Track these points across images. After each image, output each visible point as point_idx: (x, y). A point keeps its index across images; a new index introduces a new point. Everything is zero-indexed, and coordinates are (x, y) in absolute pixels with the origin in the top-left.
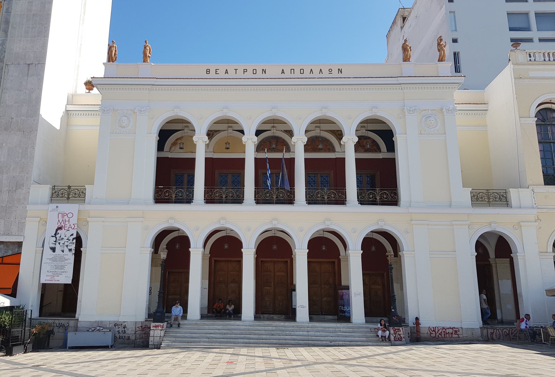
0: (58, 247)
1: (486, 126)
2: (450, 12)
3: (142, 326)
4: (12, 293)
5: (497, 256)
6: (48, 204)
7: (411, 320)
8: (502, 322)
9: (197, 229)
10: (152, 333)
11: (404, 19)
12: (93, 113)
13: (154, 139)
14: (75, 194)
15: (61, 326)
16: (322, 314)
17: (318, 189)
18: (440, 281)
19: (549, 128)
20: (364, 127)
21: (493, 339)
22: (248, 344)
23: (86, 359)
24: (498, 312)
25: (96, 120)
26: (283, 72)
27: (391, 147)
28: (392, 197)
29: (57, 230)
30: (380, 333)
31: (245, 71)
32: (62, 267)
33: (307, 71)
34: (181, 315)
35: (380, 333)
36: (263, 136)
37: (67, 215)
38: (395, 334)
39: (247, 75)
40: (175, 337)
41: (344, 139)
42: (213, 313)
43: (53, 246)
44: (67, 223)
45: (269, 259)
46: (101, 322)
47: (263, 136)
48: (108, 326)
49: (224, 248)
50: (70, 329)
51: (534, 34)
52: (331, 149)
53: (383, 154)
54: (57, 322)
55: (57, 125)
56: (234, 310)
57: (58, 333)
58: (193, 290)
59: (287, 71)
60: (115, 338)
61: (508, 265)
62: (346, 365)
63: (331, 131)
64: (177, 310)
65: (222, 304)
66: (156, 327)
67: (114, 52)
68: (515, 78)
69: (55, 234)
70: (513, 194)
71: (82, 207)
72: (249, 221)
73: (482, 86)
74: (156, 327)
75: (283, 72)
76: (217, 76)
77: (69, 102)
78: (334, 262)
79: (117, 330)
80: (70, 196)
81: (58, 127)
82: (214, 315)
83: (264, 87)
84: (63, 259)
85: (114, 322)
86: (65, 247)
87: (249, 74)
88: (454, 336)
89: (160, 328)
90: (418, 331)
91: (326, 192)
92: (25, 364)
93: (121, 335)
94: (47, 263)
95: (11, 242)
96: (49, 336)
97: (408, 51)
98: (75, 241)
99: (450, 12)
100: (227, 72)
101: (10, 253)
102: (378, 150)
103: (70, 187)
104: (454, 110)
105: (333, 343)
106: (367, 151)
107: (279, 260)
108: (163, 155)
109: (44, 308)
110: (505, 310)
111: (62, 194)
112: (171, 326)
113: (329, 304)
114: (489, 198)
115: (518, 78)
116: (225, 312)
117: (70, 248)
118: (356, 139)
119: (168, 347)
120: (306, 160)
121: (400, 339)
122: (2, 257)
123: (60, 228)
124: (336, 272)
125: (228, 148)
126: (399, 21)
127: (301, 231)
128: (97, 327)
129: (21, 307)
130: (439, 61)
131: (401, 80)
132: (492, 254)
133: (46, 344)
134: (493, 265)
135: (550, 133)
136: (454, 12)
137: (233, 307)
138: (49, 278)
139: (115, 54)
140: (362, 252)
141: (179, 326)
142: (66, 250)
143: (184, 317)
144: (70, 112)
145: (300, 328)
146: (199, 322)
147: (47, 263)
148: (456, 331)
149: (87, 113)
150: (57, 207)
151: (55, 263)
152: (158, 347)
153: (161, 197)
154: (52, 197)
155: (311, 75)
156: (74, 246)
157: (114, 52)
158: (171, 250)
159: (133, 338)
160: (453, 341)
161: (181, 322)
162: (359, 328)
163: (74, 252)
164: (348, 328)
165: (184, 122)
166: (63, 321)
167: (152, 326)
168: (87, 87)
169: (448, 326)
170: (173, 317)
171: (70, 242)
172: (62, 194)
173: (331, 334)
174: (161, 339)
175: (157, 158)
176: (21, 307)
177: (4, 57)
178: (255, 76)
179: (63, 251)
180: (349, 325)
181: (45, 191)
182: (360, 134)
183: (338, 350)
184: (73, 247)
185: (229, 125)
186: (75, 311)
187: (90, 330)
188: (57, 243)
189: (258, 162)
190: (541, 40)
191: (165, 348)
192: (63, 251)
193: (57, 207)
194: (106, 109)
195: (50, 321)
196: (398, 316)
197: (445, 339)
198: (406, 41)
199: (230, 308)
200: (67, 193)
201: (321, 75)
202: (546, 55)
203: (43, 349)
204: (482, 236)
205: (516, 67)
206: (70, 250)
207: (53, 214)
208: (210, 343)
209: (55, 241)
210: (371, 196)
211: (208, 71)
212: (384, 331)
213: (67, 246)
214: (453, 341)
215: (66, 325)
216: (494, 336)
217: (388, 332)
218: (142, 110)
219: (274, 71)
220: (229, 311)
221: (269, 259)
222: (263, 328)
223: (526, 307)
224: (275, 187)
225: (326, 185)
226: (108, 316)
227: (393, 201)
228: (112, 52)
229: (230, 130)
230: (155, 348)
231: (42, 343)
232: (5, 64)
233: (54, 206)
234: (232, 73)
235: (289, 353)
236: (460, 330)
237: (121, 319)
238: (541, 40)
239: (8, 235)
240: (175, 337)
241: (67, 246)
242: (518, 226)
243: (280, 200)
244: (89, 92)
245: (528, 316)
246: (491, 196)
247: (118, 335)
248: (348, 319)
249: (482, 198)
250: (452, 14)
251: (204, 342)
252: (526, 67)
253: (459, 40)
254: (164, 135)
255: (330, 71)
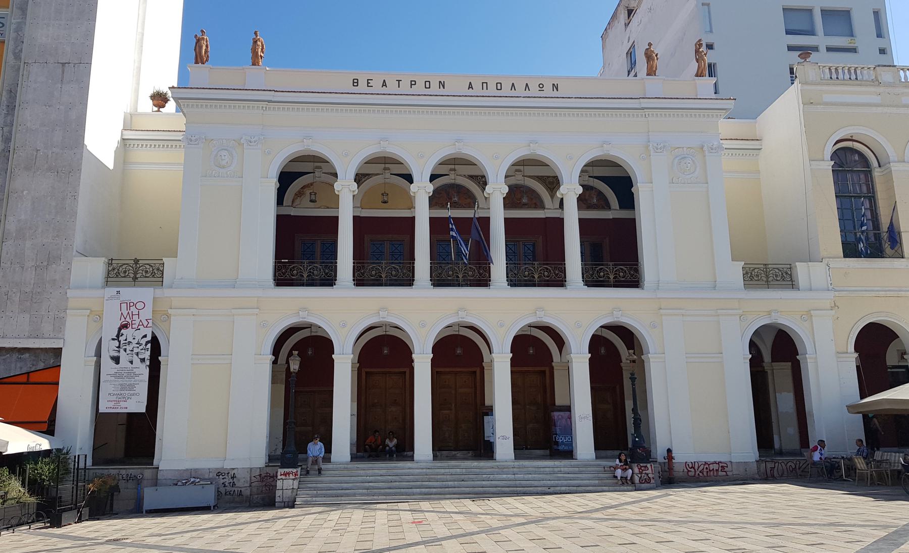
0: (122, 355)
1: (758, 172)
2: (703, 4)
3: (260, 475)
4: (48, 429)
5: (774, 359)
6: (103, 287)
7: (660, 452)
8: (781, 453)
9: (344, 326)
10: (279, 484)
11: (630, 12)
12: (170, 143)
13: (272, 185)
14: (146, 272)
15: (129, 478)
16: (527, 449)
17: (293, 263)
18: (697, 396)
19: (849, 176)
20: (519, 171)
21: (773, 476)
22: (427, 496)
23: (186, 527)
24: (776, 438)
25: (178, 156)
26: (470, 86)
27: (627, 199)
28: (632, 275)
29: (120, 329)
30: (619, 473)
31: (413, 83)
32: (131, 387)
33: (520, 87)
34: (322, 456)
35: (619, 473)
36: (440, 182)
37: (135, 305)
38: (641, 473)
39: (417, 89)
40: (315, 489)
41: (488, 189)
42: (365, 451)
43: (116, 354)
44: (135, 317)
45: (448, 370)
46: (196, 470)
47: (440, 182)
48: (207, 476)
49: (384, 354)
50: (145, 482)
51: (820, 40)
52: (538, 203)
53: (615, 212)
54: (123, 472)
55: (109, 161)
56: (397, 446)
57: (127, 491)
58: (338, 416)
59: (477, 85)
60: (219, 494)
61: (789, 372)
62: (592, 519)
63: (538, 177)
64: (315, 448)
65: (384, 437)
66: (285, 474)
67: (204, 48)
68: (804, 104)
69: (118, 336)
70: (802, 270)
71: (159, 292)
72: (422, 312)
73: (753, 115)
74: (285, 474)
75: (470, 86)
76: (369, 90)
77: (128, 125)
78: (544, 372)
79: (222, 481)
80: (770, 279)
81: (111, 166)
82: (366, 455)
83: (584, 112)
84: (131, 375)
85: (217, 469)
86: (135, 356)
87: (419, 88)
88: (720, 473)
89: (291, 477)
90: (671, 468)
91: (609, 270)
92: (92, 539)
93: (229, 489)
94: (107, 381)
95: (42, 349)
96: (112, 495)
97: (653, 60)
98: (149, 346)
99: (703, 4)
100: (384, 84)
101: (41, 365)
102: (606, 206)
103: (138, 260)
104: (720, 147)
105: (552, 489)
106: (590, 207)
107: (530, 369)
108: (286, 211)
109: (101, 452)
110: (785, 434)
111: (125, 272)
112: (308, 472)
113: (541, 433)
114: (767, 277)
115: (808, 103)
116: (383, 450)
117: (142, 357)
118: (506, 190)
119: (307, 504)
120: (507, 220)
121: (648, 481)
122: (28, 373)
123: (124, 326)
124: (548, 385)
125: (385, 202)
126: (623, 16)
127: (502, 326)
128: (190, 478)
129: (65, 451)
130: (697, 75)
131: (645, 103)
132: (767, 357)
133: (108, 508)
134: (769, 372)
135: (850, 183)
136: (708, 5)
137: (395, 441)
138: (111, 404)
139: (206, 51)
140: (856, 355)
141: (320, 473)
142: (136, 360)
143: (327, 459)
144: (128, 142)
145: (502, 469)
146: (350, 466)
147: (107, 381)
148: (723, 466)
149: (157, 143)
150: (118, 292)
151: (120, 381)
152: (291, 505)
153: (283, 278)
154: (108, 277)
155: (513, 93)
156: (149, 353)
157: (204, 48)
158: (303, 359)
159: (247, 492)
160: (719, 481)
161: (323, 467)
162: (586, 466)
163: (148, 363)
164: (572, 466)
165: (317, 160)
166: (133, 470)
167: (279, 474)
168: (156, 102)
169: (712, 460)
170: (310, 460)
171: (141, 347)
172: (125, 272)
173: (548, 477)
174: (294, 494)
175: (278, 216)
176: (65, 451)
177: (21, 51)
178: (427, 91)
179: (131, 362)
180: (573, 462)
181: (97, 267)
182: (513, 181)
183: (523, 501)
184: (147, 355)
185: (387, 166)
186: (152, 455)
187: (180, 483)
188: (122, 350)
189: (435, 223)
190: (829, 49)
191: (301, 506)
192: (131, 362)
193: (118, 292)
194: (193, 138)
195: (113, 472)
196: (644, 448)
197: (708, 479)
198: (650, 45)
199: (392, 443)
200: (133, 270)
201: (527, 93)
202: (833, 71)
203: (104, 514)
204: (757, 333)
205: (806, 87)
206: (143, 360)
207: (112, 305)
208: (370, 497)
209: (119, 347)
210: (374, 273)
211: (355, 83)
212: (625, 470)
213: (137, 354)
214: (719, 481)
215: (139, 477)
216: (776, 474)
217: (630, 471)
218: (253, 140)
219: (456, 85)
220: (391, 448)
221: (448, 370)
222: (447, 470)
223: (819, 429)
224: (461, 263)
225: (537, 257)
226: (207, 460)
227: (633, 280)
228: (201, 47)
229: (388, 175)
230: (285, 507)
231: (101, 507)
232: (22, 64)
233: (112, 291)
234: (392, 87)
235: (495, 504)
236: (729, 464)
237: (228, 465)
238: (829, 49)
239: (37, 337)
240: (315, 489)
241: (137, 354)
242: (808, 316)
243: (313, 280)
244: (159, 111)
245: (822, 443)
246: (770, 274)
247: (222, 490)
248: (569, 454)
249: (757, 276)
250: (706, 7)
251: (362, 495)
252: (819, 87)
253: (715, 46)
254: (286, 178)
255: (541, 86)
